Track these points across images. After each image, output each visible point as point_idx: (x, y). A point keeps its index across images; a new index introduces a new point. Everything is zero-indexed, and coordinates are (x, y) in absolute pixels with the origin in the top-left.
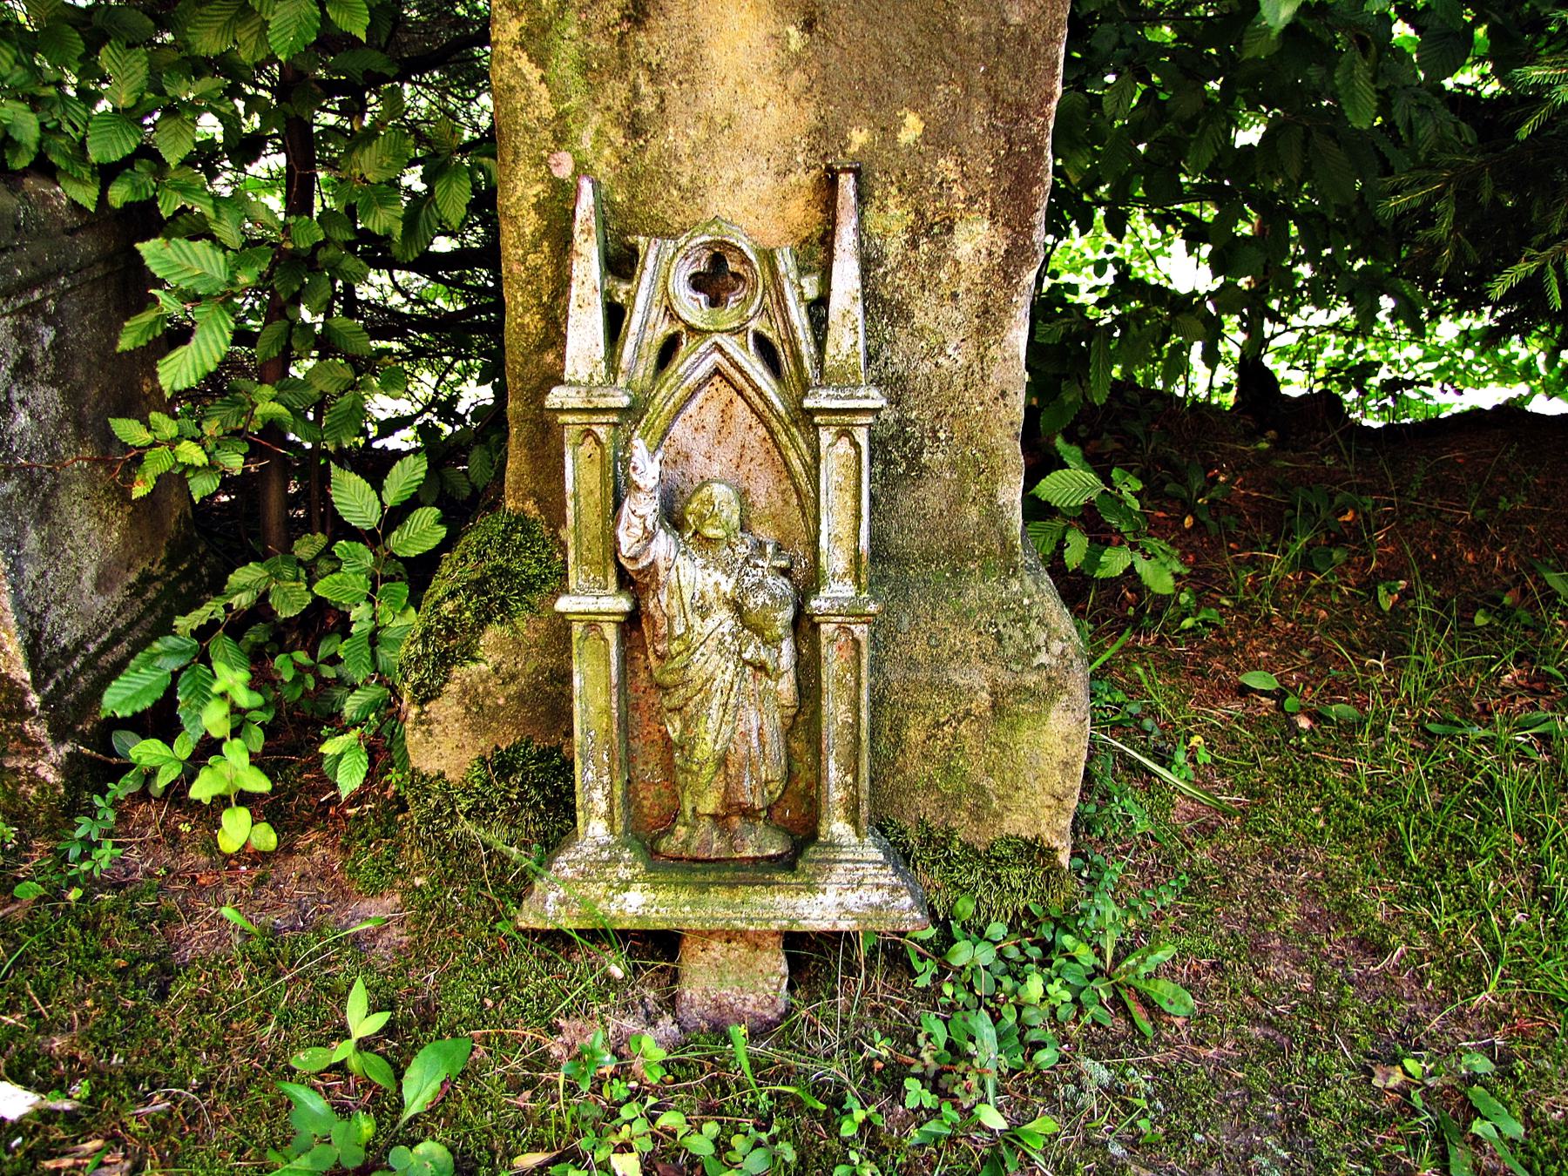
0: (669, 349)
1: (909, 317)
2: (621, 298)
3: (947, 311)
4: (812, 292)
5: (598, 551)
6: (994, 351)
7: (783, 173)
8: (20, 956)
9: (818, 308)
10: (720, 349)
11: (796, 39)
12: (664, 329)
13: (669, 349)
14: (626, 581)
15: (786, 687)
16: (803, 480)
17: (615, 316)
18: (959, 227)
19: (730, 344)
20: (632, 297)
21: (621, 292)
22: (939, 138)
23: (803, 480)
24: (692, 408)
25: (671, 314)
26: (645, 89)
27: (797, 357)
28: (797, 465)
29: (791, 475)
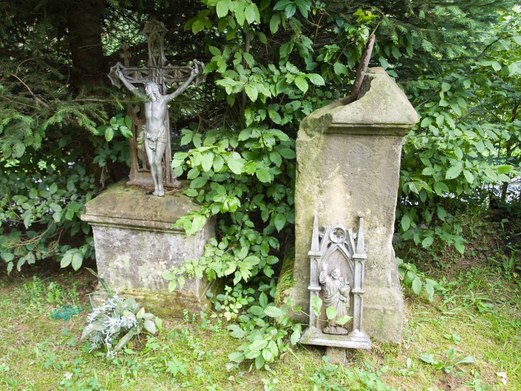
0: (329, 245)
1: (369, 242)
2: (321, 237)
3: (376, 241)
4: (355, 237)
5: (315, 279)
6: (384, 248)
7: (346, 219)
8: (18, 77)
9: (356, 240)
10: (338, 246)
11: (348, 196)
12: (329, 242)
13: (329, 245)
14: (320, 284)
15: (348, 304)
16: (352, 269)
17: (320, 239)
18: (378, 228)
19: (340, 245)
20: (323, 236)
21: (321, 235)
22: (373, 213)
23: (352, 269)
24: (333, 255)
25: (329, 238)
26: (322, 205)
27: (352, 249)
28: (351, 267)
29: (350, 268)
